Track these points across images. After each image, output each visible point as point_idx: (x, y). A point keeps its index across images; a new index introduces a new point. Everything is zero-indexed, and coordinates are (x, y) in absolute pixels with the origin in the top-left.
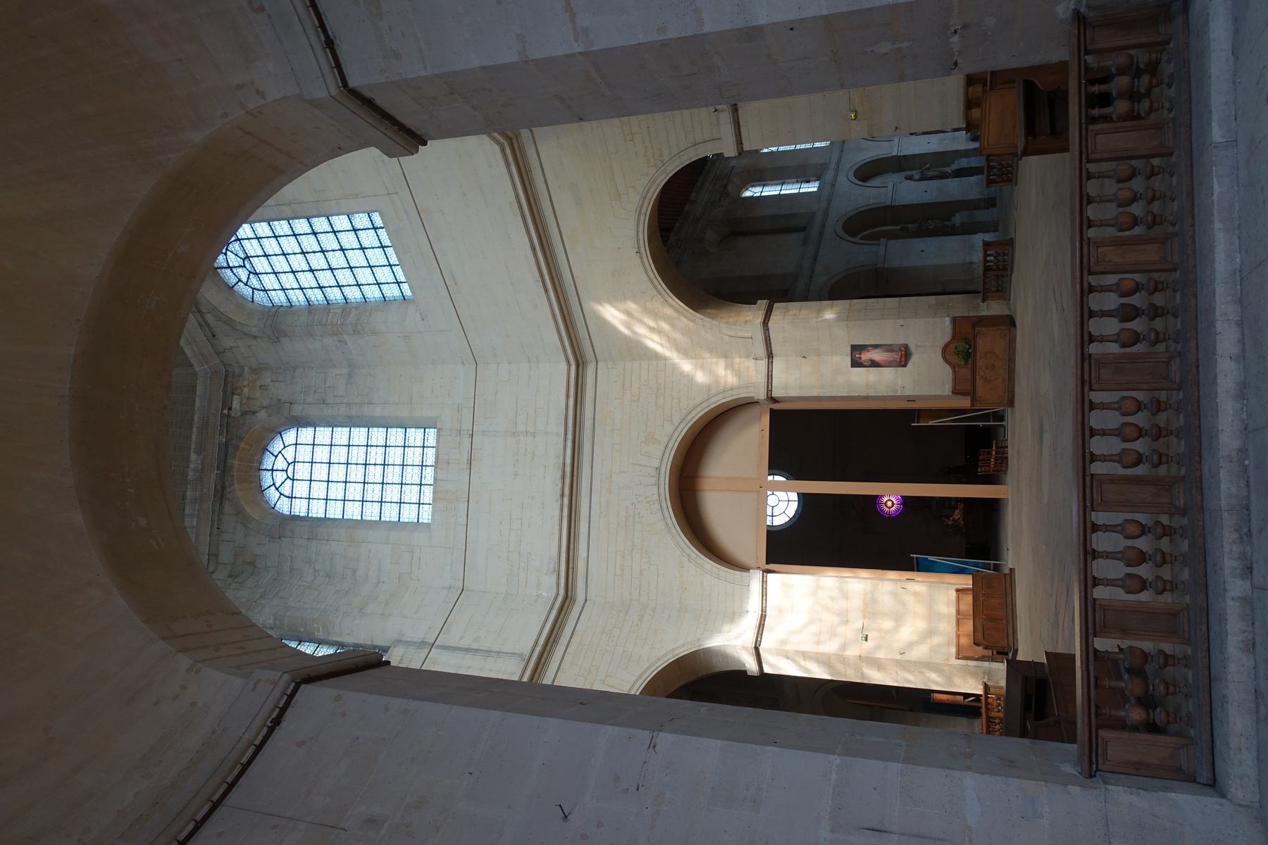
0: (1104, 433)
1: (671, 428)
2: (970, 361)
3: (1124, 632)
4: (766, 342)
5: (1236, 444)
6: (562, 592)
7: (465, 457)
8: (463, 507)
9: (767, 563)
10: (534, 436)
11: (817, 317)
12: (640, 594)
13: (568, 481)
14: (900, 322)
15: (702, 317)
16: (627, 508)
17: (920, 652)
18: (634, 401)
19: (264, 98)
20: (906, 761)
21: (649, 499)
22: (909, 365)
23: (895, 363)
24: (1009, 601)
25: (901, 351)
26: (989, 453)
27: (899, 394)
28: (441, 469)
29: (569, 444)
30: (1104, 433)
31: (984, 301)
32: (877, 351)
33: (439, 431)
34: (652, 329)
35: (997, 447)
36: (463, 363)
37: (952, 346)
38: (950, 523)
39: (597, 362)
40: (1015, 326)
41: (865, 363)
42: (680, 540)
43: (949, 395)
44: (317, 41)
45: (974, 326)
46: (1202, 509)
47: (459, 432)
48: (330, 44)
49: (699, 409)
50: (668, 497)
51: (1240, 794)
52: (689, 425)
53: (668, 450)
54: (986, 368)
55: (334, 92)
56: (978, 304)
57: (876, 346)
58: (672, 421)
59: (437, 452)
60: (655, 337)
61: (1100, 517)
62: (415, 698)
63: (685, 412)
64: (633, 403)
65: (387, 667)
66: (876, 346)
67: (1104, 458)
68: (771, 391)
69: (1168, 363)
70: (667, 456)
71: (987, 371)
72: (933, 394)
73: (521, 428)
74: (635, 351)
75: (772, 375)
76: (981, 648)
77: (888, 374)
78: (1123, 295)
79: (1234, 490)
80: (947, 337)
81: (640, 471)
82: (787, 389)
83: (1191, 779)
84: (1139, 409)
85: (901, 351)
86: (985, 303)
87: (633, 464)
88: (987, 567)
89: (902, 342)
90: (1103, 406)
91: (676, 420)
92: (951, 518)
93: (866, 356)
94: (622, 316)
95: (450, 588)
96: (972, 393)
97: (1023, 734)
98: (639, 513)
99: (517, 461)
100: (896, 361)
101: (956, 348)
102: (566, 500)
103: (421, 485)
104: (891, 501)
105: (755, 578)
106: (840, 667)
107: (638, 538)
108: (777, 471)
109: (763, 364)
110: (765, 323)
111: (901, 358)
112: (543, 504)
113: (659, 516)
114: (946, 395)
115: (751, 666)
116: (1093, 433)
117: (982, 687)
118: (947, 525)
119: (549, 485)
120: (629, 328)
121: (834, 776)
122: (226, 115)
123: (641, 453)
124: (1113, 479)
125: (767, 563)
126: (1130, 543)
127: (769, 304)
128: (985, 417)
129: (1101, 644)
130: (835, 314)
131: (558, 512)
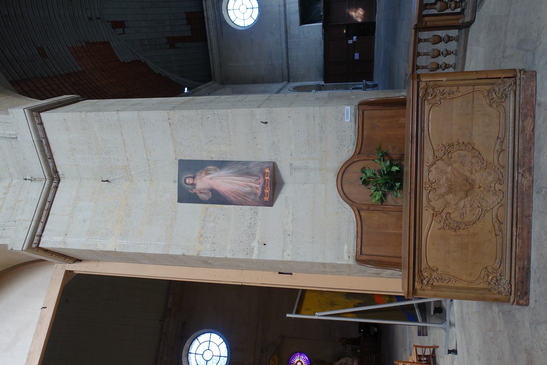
4: (43, 151)
23: (252, 197)
25: (264, 174)
27: (254, 257)
37: (357, 168)
41: (202, 196)
43: (349, 266)
54: (450, 190)
57: (221, 165)
66: (221, 165)
68: (41, 236)
71: (450, 197)
72: (320, 260)
75: (49, 209)
85: (264, 174)
100: (255, 194)
101: (363, 171)
104: (301, 362)
108: (212, 330)
111: (263, 188)
114: (342, 265)
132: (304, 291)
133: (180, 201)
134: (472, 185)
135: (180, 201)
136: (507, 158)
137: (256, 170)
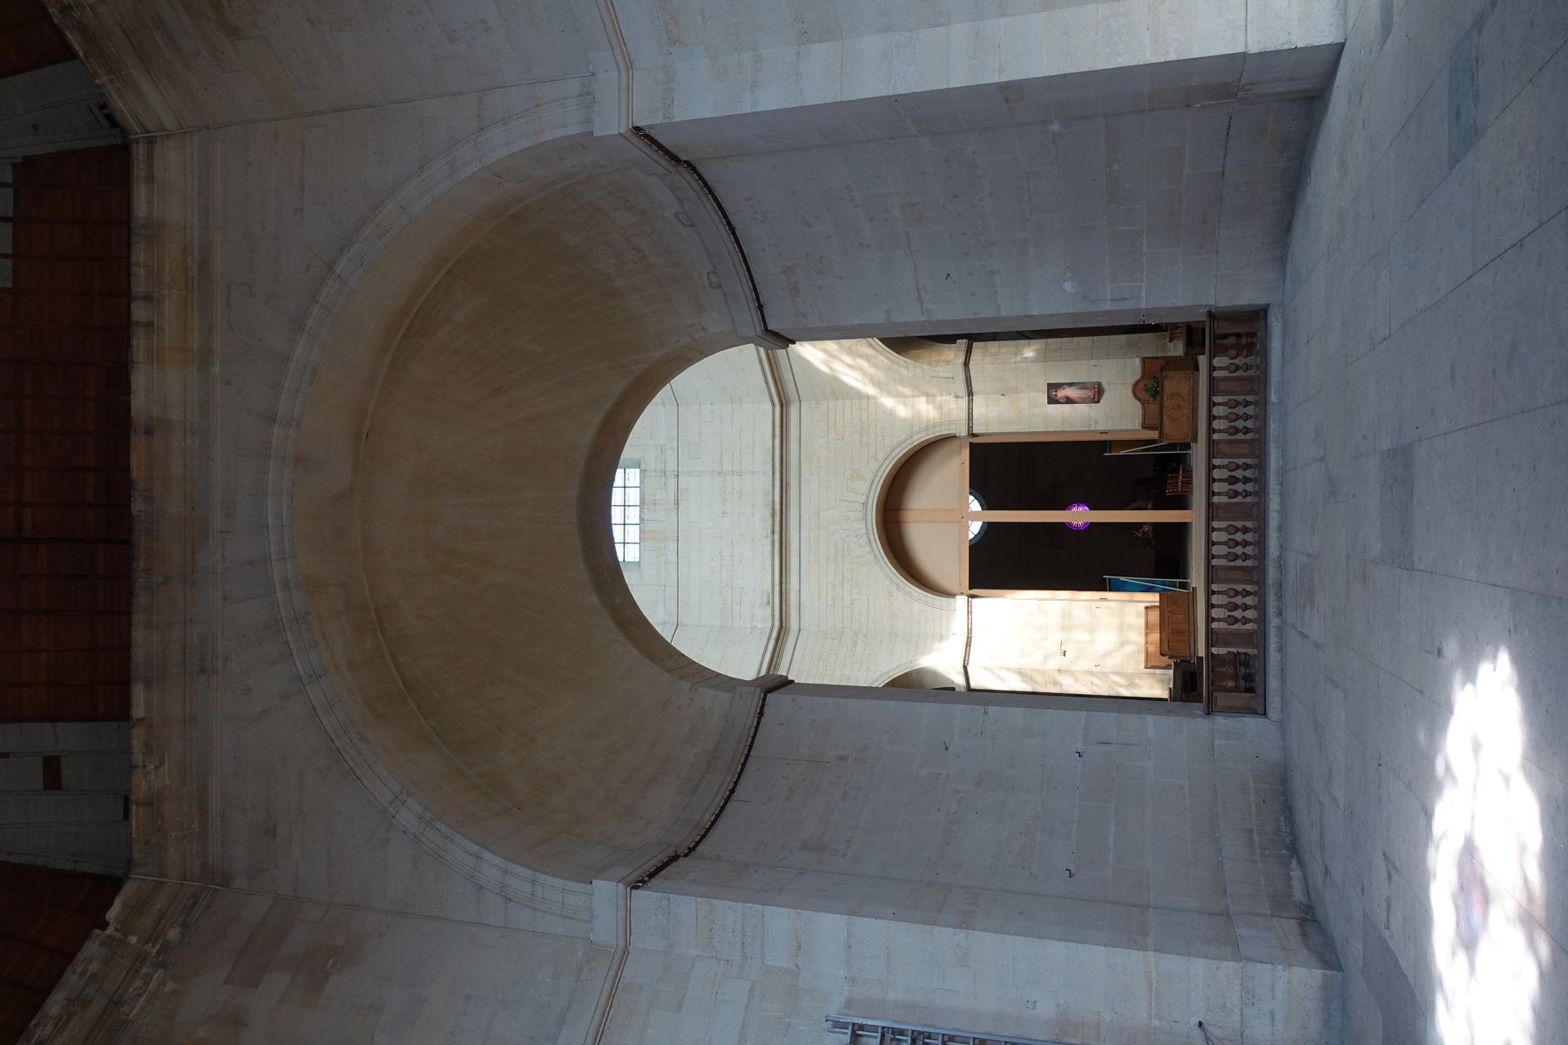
0: (1219, 543)
1: (876, 465)
2: (1158, 397)
3: (1226, 644)
4: (967, 382)
5: (1277, 554)
6: (777, 623)
7: (672, 498)
8: (672, 545)
9: (970, 589)
10: (741, 475)
11: (1016, 354)
12: (851, 623)
13: (777, 518)
14: (1094, 362)
15: (905, 359)
16: (836, 541)
17: (1113, 661)
18: (839, 439)
19: (706, 332)
20: (1118, 712)
21: (857, 533)
22: (1102, 401)
24: (1191, 616)
26: (1177, 478)
27: (1092, 429)
28: (648, 509)
29: (777, 483)
30: (1219, 543)
31: (1170, 341)
32: (1072, 388)
33: (642, 472)
34: (850, 366)
35: (1183, 472)
36: (664, 404)
38: (1140, 535)
39: (800, 401)
40: (1198, 370)
41: (1061, 401)
42: (888, 571)
44: (753, 306)
45: (1162, 369)
46: (1264, 583)
47: (664, 473)
48: (760, 307)
49: (903, 446)
50: (875, 530)
51: (1273, 716)
52: (894, 462)
53: (874, 487)
54: (1173, 409)
55: (759, 333)
56: (1165, 344)
57: (1071, 385)
58: (876, 457)
59: (642, 493)
60: (850, 372)
61: (1215, 587)
62: (841, 697)
63: (888, 449)
64: (838, 442)
65: (791, 685)
66: (1071, 385)
67: (1219, 557)
69: (1251, 508)
70: (873, 491)
73: (727, 467)
74: (836, 390)
76: (1166, 657)
77: (1081, 408)
78: (1230, 471)
79: (1275, 576)
80: (1138, 376)
81: (848, 507)
82: (986, 426)
83: (1255, 713)
84: (1237, 532)
86: (1172, 344)
87: (840, 500)
88: (1173, 585)
89: (1094, 379)
90: (1218, 530)
91: (881, 457)
92: (1141, 531)
93: (1061, 393)
94: (821, 355)
95: (664, 624)
96: (1159, 427)
97: (1182, 700)
98: (848, 547)
99: (725, 499)
101: (1145, 385)
102: (777, 537)
103: (624, 524)
105: (961, 600)
106: (1040, 679)
107: (848, 570)
109: (964, 402)
110: (966, 364)
112: (753, 541)
113: (868, 549)
115: (959, 680)
116: (1214, 543)
117: (1168, 692)
118: (1137, 538)
119: (759, 521)
120: (827, 365)
121: (1083, 721)
122: (679, 341)
123: (847, 489)
124: (1223, 568)
125: (970, 589)
126: (1230, 600)
127: (968, 344)
128: (1172, 446)
129: (1214, 650)
130: (1035, 351)
131: (769, 548)
132: (1111, 441)
133: (1049, 403)
134: (1179, 406)
135: (1049, 403)
136: (1191, 398)
137: (1090, 386)
